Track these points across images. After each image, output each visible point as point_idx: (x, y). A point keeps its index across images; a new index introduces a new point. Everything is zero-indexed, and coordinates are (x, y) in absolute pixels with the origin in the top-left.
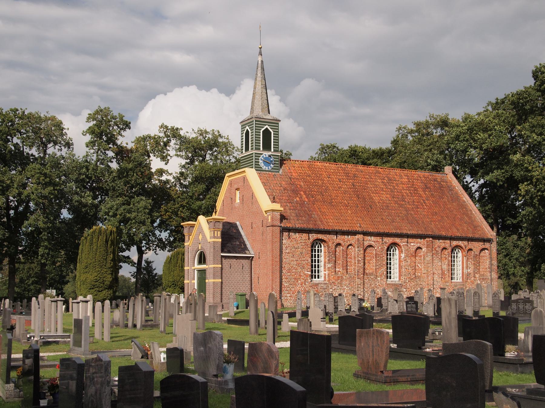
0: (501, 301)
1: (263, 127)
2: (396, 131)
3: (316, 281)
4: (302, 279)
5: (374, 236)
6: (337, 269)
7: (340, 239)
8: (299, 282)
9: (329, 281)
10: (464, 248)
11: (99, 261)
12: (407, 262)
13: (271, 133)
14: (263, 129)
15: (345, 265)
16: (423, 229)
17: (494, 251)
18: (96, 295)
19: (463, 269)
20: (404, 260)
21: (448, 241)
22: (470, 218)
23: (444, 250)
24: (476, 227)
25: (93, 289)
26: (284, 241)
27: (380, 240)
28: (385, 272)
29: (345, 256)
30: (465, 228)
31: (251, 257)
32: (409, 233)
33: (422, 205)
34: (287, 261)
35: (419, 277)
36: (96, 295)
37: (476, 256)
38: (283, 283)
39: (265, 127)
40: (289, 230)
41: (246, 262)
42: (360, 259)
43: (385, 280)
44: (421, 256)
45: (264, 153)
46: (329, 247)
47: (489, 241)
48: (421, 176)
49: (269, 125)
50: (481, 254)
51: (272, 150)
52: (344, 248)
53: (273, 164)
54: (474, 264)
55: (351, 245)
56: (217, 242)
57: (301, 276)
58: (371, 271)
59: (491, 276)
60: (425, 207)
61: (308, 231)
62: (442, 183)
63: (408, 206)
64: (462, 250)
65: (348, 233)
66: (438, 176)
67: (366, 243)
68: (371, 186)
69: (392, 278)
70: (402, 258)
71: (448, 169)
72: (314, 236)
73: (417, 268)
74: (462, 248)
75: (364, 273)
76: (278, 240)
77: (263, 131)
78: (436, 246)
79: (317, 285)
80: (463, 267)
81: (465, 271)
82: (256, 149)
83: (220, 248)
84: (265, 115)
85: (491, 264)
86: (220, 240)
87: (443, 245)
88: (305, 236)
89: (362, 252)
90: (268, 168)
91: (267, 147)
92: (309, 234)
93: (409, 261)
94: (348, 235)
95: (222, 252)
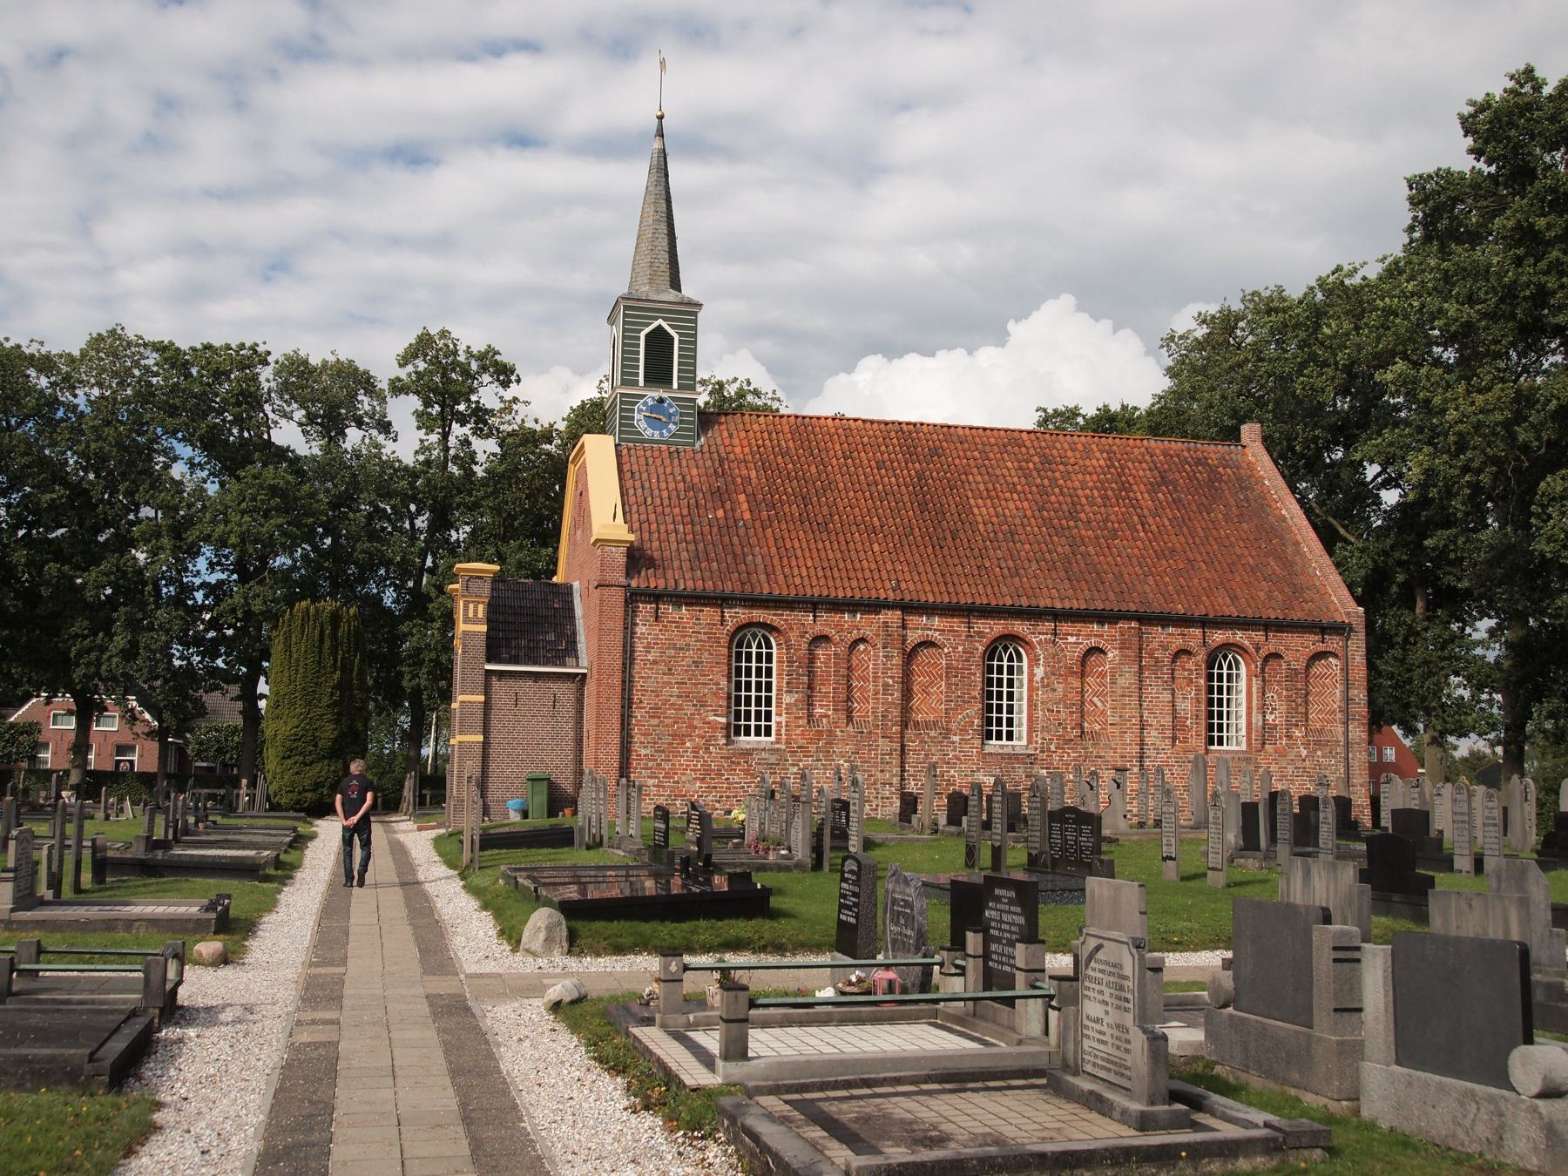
0: (1295, 814)
1: (648, 325)
2: (1162, 347)
3: (748, 742)
4: (698, 736)
5: (940, 615)
6: (818, 711)
7: (826, 622)
8: (688, 744)
9: (787, 742)
10: (1252, 649)
11: (304, 689)
12: (1054, 690)
13: (672, 339)
14: (648, 330)
15: (843, 697)
16: (1112, 596)
17: (1359, 658)
18: (297, 773)
19: (1249, 714)
20: (1043, 686)
21: (1197, 632)
22: (1286, 563)
23: (1184, 658)
24: (1297, 588)
25: (289, 757)
26: (640, 630)
27: (963, 628)
28: (976, 721)
29: (843, 672)
30: (1261, 594)
31: (578, 674)
32: (1058, 605)
33: (1133, 528)
34: (651, 685)
35: (1095, 736)
36: (297, 773)
37: (1292, 675)
38: (636, 747)
39: (656, 324)
40: (656, 597)
41: (565, 691)
42: (890, 681)
43: (977, 742)
44: (1102, 675)
45: (650, 394)
46: (789, 647)
47: (1341, 629)
48: (1157, 451)
49: (665, 319)
50: (1314, 670)
51: (675, 386)
52: (842, 650)
53: (675, 423)
54: (1289, 699)
55: (863, 640)
56: (474, 634)
57: (692, 727)
58: (932, 717)
59: (1347, 733)
60: (1142, 534)
61: (721, 601)
62: (1220, 469)
63: (1083, 532)
64: (1247, 657)
65: (853, 605)
66: (1215, 451)
67: (913, 637)
68: (979, 478)
69: (1015, 735)
70: (1038, 678)
71: (1250, 432)
72: (741, 614)
73: (1088, 707)
74: (1247, 652)
75: (904, 725)
76: (619, 625)
77: (647, 336)
78: (1155, 645)
79: (747, 753)
80: (1249, 708)
81: (1257, 719)
82: (624, 383)
83: (483, 649)
84: (658, 292)
85: (1347, 700)
86: (484, 628)
87: (1178, 643)
88: (709, 614)
89: (897, 660)
90: (661, 435)
91: (658, 372)
92: (721, 606)
93: (1060, 688)
94: (853, 612)
95: (489, 661)
